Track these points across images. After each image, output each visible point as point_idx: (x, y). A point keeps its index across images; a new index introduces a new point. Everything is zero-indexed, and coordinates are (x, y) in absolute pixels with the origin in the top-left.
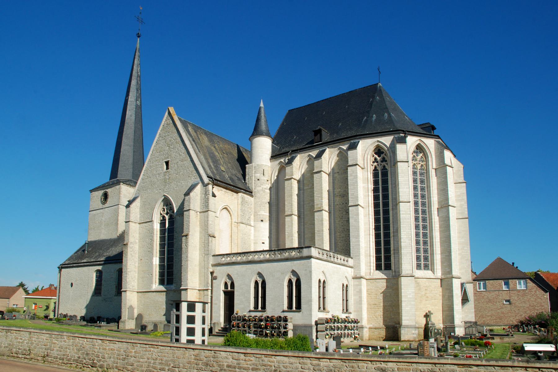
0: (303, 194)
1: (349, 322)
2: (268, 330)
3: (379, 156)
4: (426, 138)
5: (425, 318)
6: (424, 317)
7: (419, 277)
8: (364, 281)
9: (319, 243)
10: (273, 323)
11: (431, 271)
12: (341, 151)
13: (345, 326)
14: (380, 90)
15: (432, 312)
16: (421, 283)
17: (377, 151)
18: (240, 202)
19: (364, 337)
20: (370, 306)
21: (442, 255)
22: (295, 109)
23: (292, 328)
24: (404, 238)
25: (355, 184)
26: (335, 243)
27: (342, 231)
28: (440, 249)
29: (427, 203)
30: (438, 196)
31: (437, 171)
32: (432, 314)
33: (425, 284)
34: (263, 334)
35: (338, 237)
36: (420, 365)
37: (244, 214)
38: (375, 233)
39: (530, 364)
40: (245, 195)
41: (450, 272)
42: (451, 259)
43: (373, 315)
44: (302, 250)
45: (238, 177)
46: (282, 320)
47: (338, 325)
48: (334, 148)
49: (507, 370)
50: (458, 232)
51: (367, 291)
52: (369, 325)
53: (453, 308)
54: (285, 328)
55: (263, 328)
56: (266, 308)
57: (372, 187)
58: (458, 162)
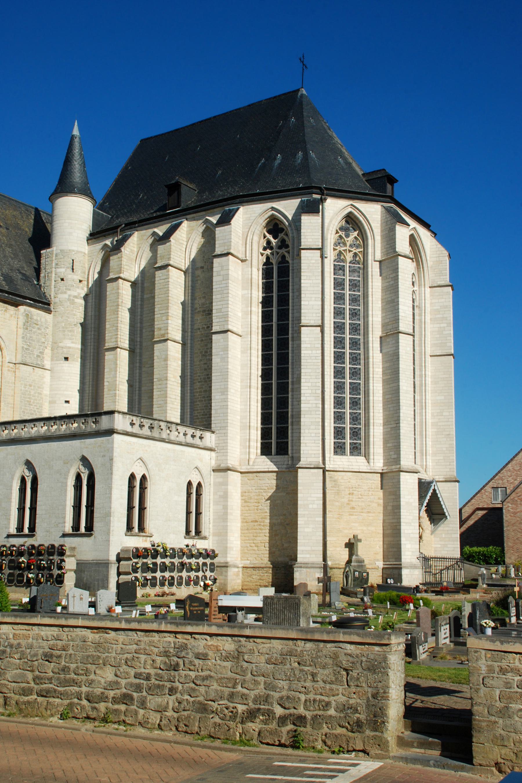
0: (142, 308)
1: (191, 556)
2: (32, 571)
3: (275, 238)
4: (364, 202)
5: (347, 549)
6: (346, 547)
7: (338, 469)
8: (234, 478)
9: (159, 403)
10: (41, 558)
11: (364, 458)
12: (209, 226)
13: (183, 564)
14: (301, 103)
15: (359, 538)
16: (342, 481)
17: (271, 227)
18: (21, 324)
19: (229, 586)
20: (245, 524)
21: (386, 427)
22: (151, 137)
23: (74, 567)
24: (306, 395)
25: (225, 292)
26: (192, 402)
27: (204, 379)
28: (382, 415)
29: (362, 327)
30: (382, 313)
31: (382, 265)
32: (360, 541)
34: (23, 580)
35: (198, 390)
36: (43, 628)
37: (29, 346)
38: (262, 384)
39: (179, 627)
40: (33, 310)
41: (397, 460)
42: (400, 436)
43: (252, 541)
44: (99, 417)
45: (24, 275)
46: (56, 553)
47: (163, 560)
48: (198, 220)
49: (152, 637)
50: (431, 382)
51: (242, 496)
52: (243, 562)
53: (400, 530)
54: (60, 568)
55: (23, 569)
56: (36, 529)
57: (261, 295)
58: (439, 246)
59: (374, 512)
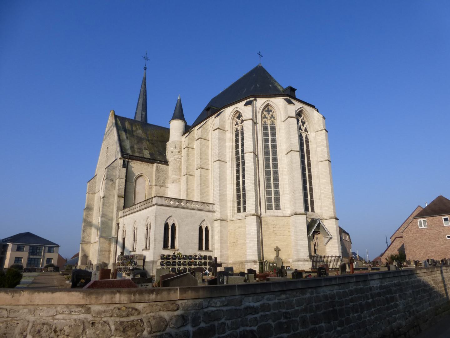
33: (273, 222)
40: (160, 165)
59: (286, 235)
